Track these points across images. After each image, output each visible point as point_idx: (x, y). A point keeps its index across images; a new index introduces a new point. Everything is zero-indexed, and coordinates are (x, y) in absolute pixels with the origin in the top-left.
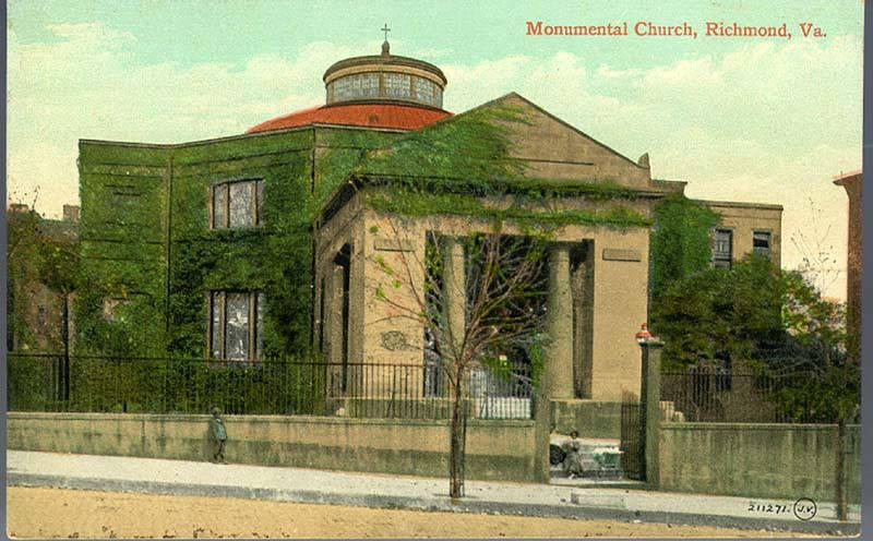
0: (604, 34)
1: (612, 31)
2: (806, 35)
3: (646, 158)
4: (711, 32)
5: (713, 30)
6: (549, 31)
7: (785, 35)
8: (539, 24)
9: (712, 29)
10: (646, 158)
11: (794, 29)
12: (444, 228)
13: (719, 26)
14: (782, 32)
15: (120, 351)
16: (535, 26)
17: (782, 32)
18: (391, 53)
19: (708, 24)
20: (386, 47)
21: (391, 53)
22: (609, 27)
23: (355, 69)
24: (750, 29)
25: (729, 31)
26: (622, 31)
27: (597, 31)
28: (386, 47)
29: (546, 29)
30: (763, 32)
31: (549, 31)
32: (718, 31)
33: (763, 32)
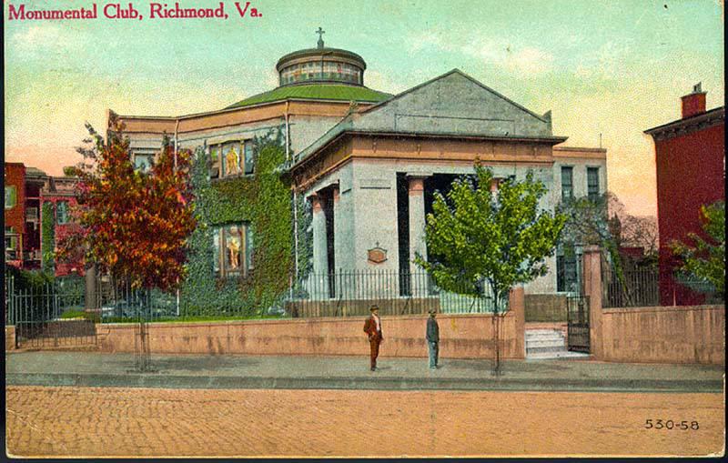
0: (78, 17)
1: (85, 14)
2: (242, 14)
3: (548, 115)
4: (156, 14)
5: (158, 11)
6: (30, 15)
7: (222, 15)
8: (22, 7)
9: (155, 10)
10: (548, 115)
11: (230, 9)
12: (411, 169)
13: (164, 8)
14: (219, 13)
15: (96, 243)
16: (17, 10)
17: (219, 13)
18: (326, 46)
19: (152, 5)
20: (321, 43)
21: (326, 46)
22: (83, 11)
23: (292, 62)
24: (57, 13)
25: (172, 14)
26: (93, 15)
27: (175, 14)
28: (321, 43)
29: (27, 15)
30: (201, 13)
31: (30, 15)
32: (162, 12)
33: (201, 13)
